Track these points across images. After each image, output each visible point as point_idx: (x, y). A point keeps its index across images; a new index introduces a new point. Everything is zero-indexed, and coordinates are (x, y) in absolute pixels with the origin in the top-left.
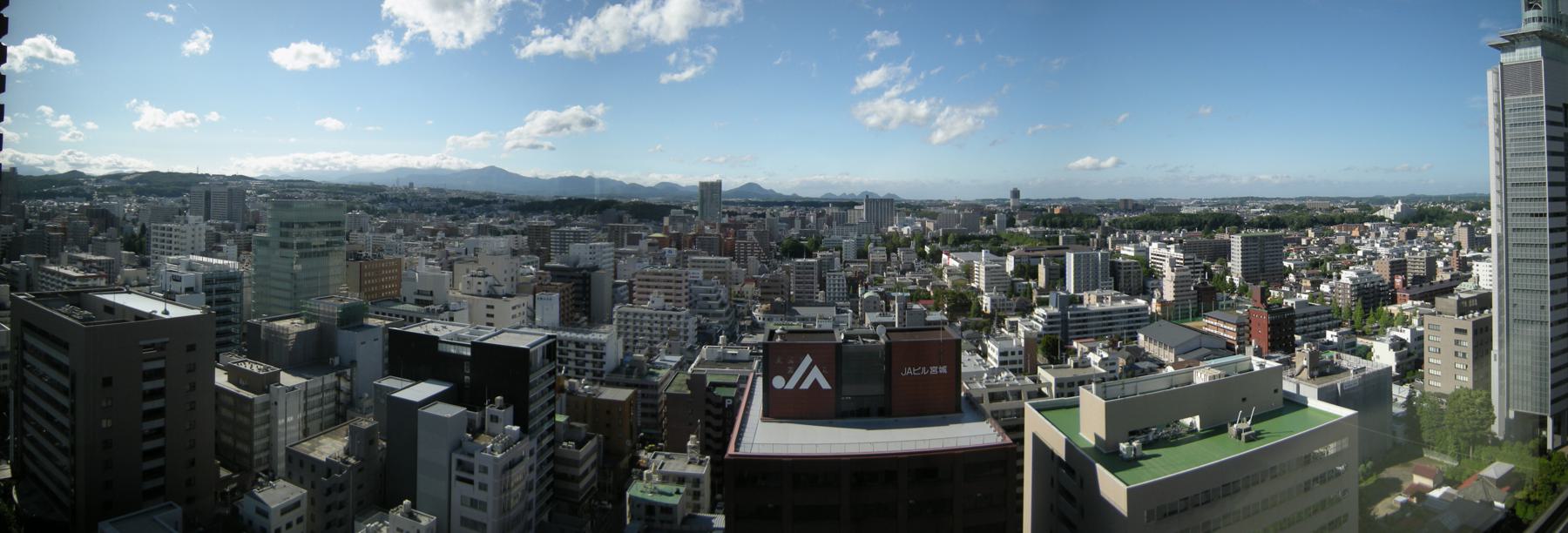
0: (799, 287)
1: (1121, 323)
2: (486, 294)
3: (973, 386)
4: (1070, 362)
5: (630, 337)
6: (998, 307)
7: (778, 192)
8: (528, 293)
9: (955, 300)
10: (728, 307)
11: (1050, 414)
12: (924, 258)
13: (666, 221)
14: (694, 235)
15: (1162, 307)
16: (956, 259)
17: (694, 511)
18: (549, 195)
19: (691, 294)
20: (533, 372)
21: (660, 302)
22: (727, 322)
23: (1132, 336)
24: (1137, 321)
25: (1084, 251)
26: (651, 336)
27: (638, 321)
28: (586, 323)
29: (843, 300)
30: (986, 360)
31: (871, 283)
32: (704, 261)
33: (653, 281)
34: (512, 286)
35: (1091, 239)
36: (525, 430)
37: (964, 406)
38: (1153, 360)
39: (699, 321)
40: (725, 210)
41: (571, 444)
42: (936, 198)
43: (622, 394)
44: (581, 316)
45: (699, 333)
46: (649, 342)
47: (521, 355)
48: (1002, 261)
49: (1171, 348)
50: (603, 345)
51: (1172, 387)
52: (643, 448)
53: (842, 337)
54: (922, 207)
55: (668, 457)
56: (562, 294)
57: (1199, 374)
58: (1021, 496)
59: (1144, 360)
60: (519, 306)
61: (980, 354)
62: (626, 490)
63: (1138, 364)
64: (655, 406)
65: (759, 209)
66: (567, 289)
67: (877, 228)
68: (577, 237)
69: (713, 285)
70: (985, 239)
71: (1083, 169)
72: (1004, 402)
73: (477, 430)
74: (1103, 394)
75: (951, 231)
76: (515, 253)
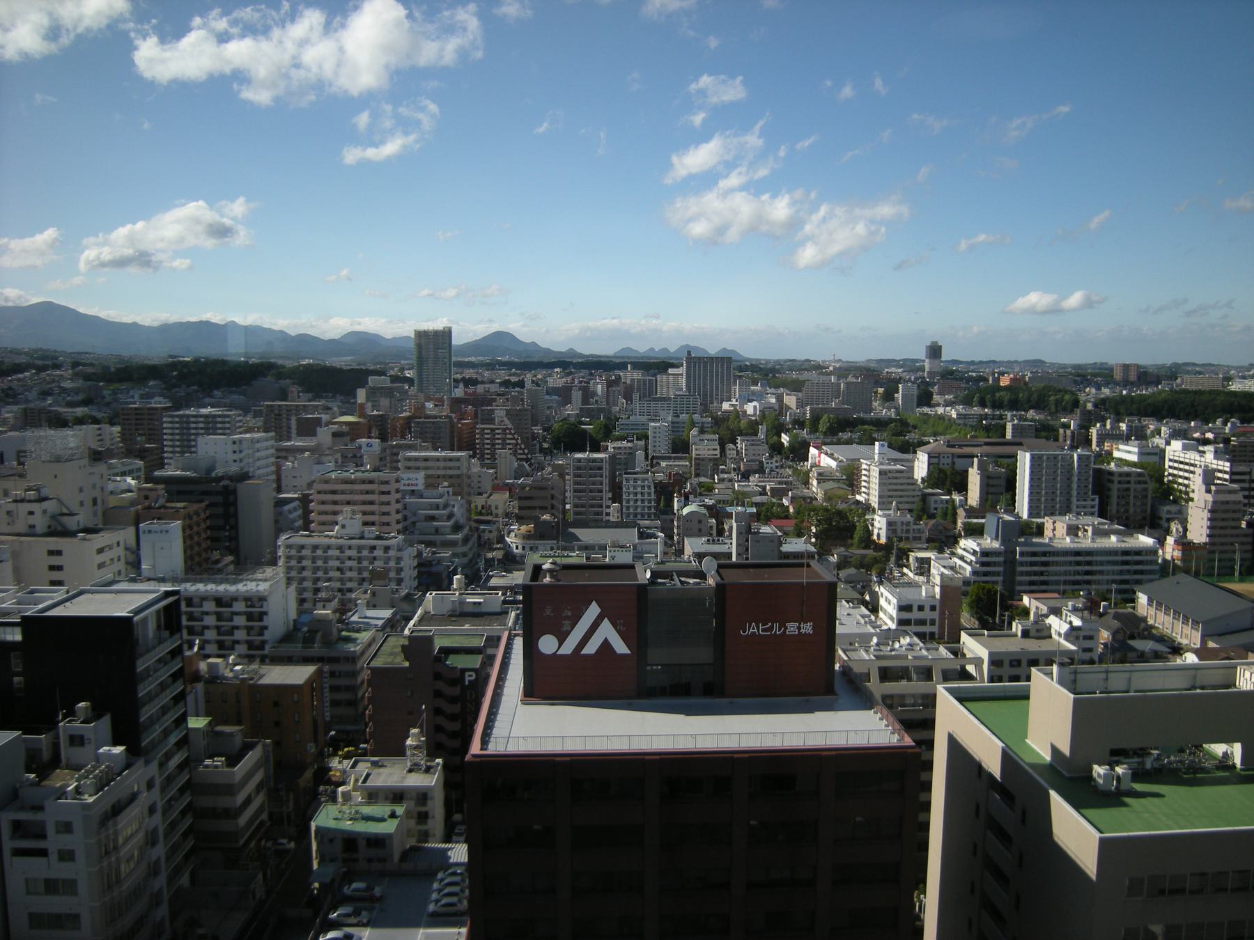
0: (579, 498)
1: (1108, 573)
2: (45, 530)
3: (853, 655)
4: (1017, 627)
5: (306, 584)
6: (899, 534)
7: (544, 346)
8: (127, 525)
9: (829, 521)
10: (466, 530)
11: (979, 706)
12: (780, 453)
13: (361, 395)
14: (409, 418)
15: (1183, 551)
16: (831, 456)
17: (419, 841)
18: (157, 354)
19: (405, 512)
20: (142, 655)
21: (355, 526)
22: (465, 555)
23: (1126, 596)
24: (1136, 572)
25: (1049, 450)
26: (341, 580)
27: (319, 558)
28: (231, 567)
29: (649, 518)
30: (877, 617)
31: (693, 492)
32: (426, 459)
33: (343, 492)
34: (95, 514)
35: (1061, 431)
36: (135, 751)
37: (838, 684)
38: (1162, 639)
39: (420, 554)
40: (459, 376)
41: (220, 761)
42: (801, 356)
43: (298, 675)
44: (223, 555)
45: (419, 572)
46: (340, 590)
47: (120, 627)
48: (908, 461)
49: (1196, 623)
50: (262, 599)
51: (1194, 688)
52: (335, 754)
53: (648, 575)
54: (778, 371)
55: (375, 764)
56: (188, 522)
57: (1247, 674)
58: (925, 827)
59: (1144, 638)
60: (110, 547)
61: (867, 608)
62: (310, 819)
63: (1132, 643)
64: (353, 689)
65: (514, 374)
66: (197, 513)
67: (704, 405)
68: (211, 426)
69: (441, 496)
70: (881, 424)
71: (1032, 311)
72: (904, 683)
73: (45, 765)
74: (1071, 683)
75: (825, 410)
76: (97, 456)
